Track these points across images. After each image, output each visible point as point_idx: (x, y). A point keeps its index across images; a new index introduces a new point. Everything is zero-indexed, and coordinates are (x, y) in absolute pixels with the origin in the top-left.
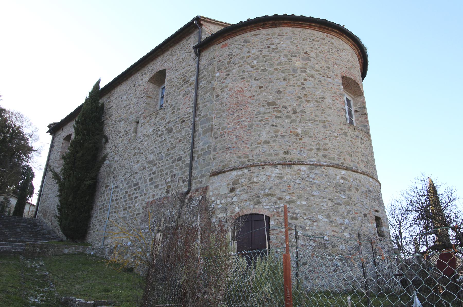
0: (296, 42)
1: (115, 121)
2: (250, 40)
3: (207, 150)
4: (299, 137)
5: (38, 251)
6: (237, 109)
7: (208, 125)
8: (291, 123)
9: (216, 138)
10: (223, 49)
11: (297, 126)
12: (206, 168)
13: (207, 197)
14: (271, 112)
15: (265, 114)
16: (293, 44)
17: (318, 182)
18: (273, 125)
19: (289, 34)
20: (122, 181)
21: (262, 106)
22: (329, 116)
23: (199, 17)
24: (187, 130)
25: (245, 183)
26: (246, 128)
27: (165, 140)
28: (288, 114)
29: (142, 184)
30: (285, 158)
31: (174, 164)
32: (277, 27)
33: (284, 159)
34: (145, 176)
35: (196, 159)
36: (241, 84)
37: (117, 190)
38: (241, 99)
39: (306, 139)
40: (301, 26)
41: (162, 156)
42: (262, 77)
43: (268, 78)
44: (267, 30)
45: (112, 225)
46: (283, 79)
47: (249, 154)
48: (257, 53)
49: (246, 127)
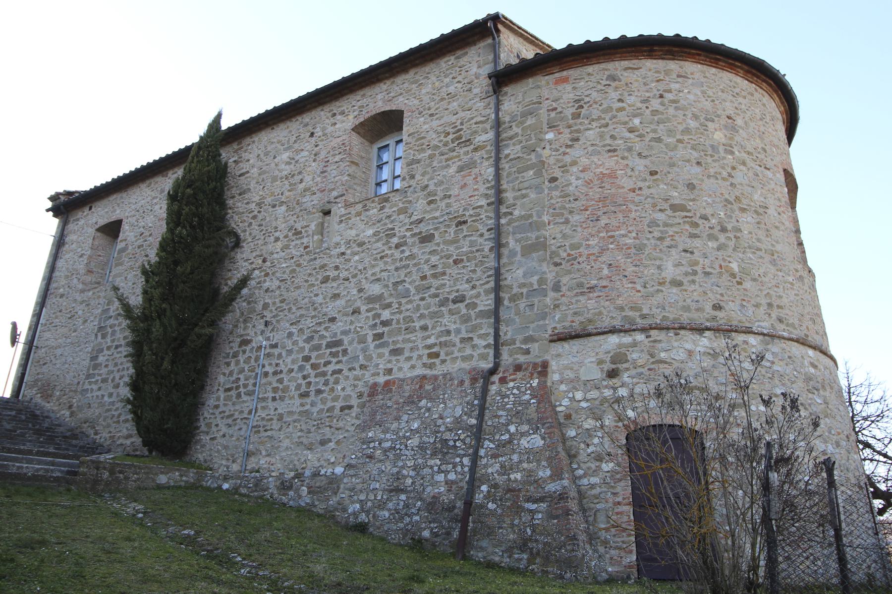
0: (711, 94)
1: (259, 205)
2: (621, 77)
3: (536, 287)
4: (735, 278)
5: (105, 476)
6: (605, 210)
7: (534, 237)
8: (718, 249)
9: (557, 264)
10: (560, 88)
11: (729, 256)
12: (536, 323)
13: (549, 384)
14: (680, 224)
15: (667, 226)
16: (706, 96)
17: (779, 369)
18: (685, 251)
19: (697, 76)
20: (290, 335)
21: (660, 210)
22: (777, 242)
23: (501, 16)
24: (476, 241)
25: (640, 362)
26: (629, 251)
27: (412, 257)
28: (711, 231)
29: (351, 343)
30: (716, 317)
31: (443, 308)
32: (674, 59)
33: (714, 318)
34: (361, 328)
35: (506, 302)
36: (610, 163)
37: (276, 351)
38: (613, 190)
39: (748, 284)
40: (717, 64)
41: (408, 290)
42: (654, 152)
43: (667, 157)
44: (655, 61)
45: (268, 428)
46: (695, 161)
47: (643, 303)
48: (639, 105)
49: (629, 248)
